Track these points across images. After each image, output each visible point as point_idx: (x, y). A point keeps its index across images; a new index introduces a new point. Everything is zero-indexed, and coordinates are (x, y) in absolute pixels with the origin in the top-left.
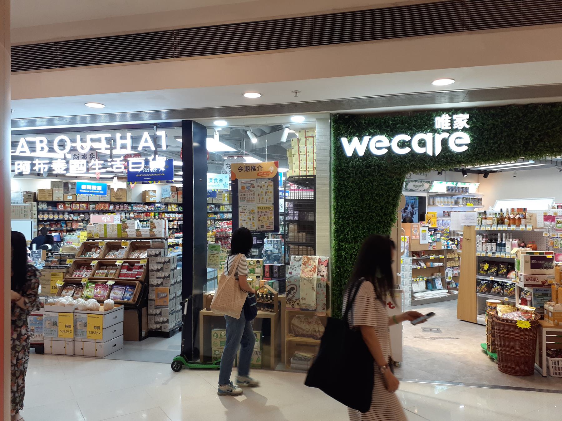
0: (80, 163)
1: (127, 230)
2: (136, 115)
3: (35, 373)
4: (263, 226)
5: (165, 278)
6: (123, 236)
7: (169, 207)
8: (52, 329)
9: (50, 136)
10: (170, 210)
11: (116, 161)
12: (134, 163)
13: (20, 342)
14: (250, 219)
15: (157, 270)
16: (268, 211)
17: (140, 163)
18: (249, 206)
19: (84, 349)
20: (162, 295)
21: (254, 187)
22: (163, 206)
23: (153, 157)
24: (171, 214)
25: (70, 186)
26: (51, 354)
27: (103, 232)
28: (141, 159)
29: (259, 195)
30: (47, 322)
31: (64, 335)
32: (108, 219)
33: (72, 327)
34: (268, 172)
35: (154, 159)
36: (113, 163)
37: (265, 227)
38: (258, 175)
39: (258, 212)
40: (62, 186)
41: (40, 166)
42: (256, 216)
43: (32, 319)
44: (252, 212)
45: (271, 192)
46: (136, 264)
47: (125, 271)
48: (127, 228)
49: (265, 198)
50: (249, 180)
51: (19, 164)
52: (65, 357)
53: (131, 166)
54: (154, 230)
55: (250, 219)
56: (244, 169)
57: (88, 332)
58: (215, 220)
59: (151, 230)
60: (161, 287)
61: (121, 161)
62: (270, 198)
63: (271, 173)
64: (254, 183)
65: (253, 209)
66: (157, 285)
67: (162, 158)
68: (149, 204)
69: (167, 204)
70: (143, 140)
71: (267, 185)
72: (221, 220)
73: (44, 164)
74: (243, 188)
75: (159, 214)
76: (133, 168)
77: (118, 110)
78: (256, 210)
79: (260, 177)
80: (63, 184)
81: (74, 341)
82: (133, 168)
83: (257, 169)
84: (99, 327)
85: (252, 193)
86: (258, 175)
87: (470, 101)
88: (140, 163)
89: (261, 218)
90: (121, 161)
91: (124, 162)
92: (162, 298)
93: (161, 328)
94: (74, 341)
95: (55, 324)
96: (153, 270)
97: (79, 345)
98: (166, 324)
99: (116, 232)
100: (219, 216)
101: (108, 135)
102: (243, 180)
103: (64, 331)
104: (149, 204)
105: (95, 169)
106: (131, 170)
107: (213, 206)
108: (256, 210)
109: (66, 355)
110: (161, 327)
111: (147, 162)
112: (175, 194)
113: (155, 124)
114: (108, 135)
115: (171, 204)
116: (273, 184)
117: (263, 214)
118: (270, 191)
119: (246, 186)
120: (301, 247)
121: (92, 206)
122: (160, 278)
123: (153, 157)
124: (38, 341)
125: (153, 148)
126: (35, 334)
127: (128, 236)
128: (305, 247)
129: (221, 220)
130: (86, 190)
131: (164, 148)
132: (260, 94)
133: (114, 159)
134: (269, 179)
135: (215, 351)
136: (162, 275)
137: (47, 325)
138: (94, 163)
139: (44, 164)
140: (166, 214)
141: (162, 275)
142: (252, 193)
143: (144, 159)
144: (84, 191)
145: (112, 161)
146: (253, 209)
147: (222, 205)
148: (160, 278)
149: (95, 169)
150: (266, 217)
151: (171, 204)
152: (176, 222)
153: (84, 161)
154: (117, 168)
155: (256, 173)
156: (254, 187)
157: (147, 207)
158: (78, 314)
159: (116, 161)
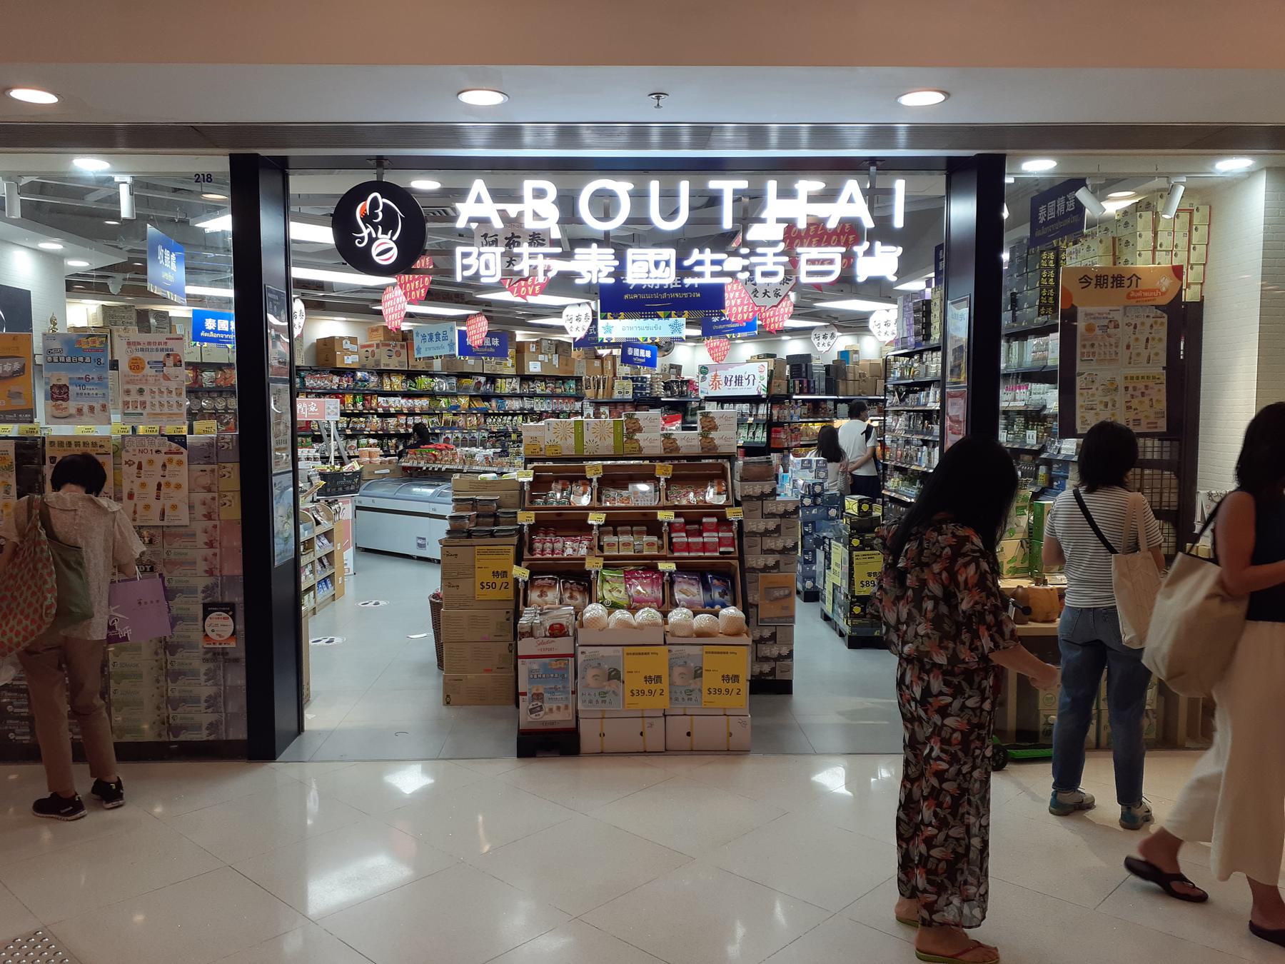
0: (658, 258)
1: (638, 436)
2: (824, 133)
3: (158, 810)
4: (1137, 422)
5: (784, 551)
6: (628, 448)
7: (386, 380)
8: (692, 687)
9: (570, 178)
10: (387, 388)
11: (764, 255)
12: (811, 262)
14: (1106, 406)
15: (767, 533)
16: (1151, 384)
17: (831, 262)
18: (1104, 374)
19: (694, 734)
20: (777, 593)
21: (1117, 326)
22: (374, 379)
23: (866, 245)
24: (391, 400)
25: (152, 321)
26: (602, 753)
27: (571, 441)
28: (835, 253)
29: (1128, 347)
30: (591, 672)
31: (645, 703)
32: (312, 409)
33: (665, 679)
34: (1154, 290)
35: (870, 252)
36: (754, 259)
37: (1144, 422)
38: (1129, 297)
39: (1126, 388)
40: (134, 320)
41: (533, 262)
42: (1121, 398)
43: (535, 667)
44: (1111, 388)
45: (1160, 340)
46: (704, 520)
47: (679, 538)
48: (640, 430)
49: (1145, 353)
50: (1106, 309)
51: (465, 255)
52: (642, 759)
53: (804, 267)
54: (713, 434)
55: (1106, 406)
56: (1094, 282)
57: (705, 692)
58: (487, 414)
59: (704, 435)
60: (773, 575)
61: (775, 255)
62: (1157, 354)
63: (1163, 294)
64: (1118, 316)
65: (1112, 381)
66: (766, 569)
67: (892, 248)
68: (340, 372)
69: (380, 373)
71: (1149, 322)
72: (499, 415)
73: (546, 255)
74: (1090, 329)
75: (364, 399)
76: (810, 274)
77: (774, 116)
78: (1121, 383)
79: (1133, 302)
80: (134, 316)
81: (665, 716)
82: (810, 274)
83: (1127, 283)
84: (659, 677)
85: (1113, 341)
86: (1129, 297)
87: (751, 147)
88: (831, 262)
89: (1135, 403)
90: (775, 255)
91: (786, 259)
92: (777, 599)
93: (773, 671)
94: (665, 716)
95: (614, 675)
96: (754, 534)
97: (678, 726)
98: (787, 662)
99: (610, 441)
100: (494, 403)
101: (743, 184)
102: (1090, 309)
103: (720, 691)
104: (340, 372)
105: (700, 275)
106: (804, 279)
107: (483, 379)
108: (1121, 383)
109: (645, 753)
110: (773, 670)
111: (849, 259)
112: (402, 347)
113: (873, 160)
114: (743, 184)
115: (389, 373)
116: (1165, 320)
117: (1138, 393)
118: (1157, 337)
119: (1097, 323)
120: (1147, 472)
121: (207, 376)
122: (771, 551)
123: (866, 245)
124: (553, 723)
125: (868, 223)
126: (546, 706)
127: (640, 449)
128: (1156, 472)
129: (499, 415)
130: (216, 331)
131: (899, 222)
133: (759, 250)
134: (1157, 307)
135: (1047, 716)
136: (778, 543)
137: (590, 680)
138: (700, 257)
139: (546, 255)
140: (380, 399)
141: (770, 543)
142: (1113, 341)
143: (843, 250)
144: (212, 334)
145: (753, 253)
146: (1112, 381)
147: (501, 376)
148: (771, 551)
149: (700, 275)
150: (1146, 399)
151: (389, 373)
152: (402, 419)
153: (670, 254)
154: (764, 274)
155: (1122, 292)
156: (1117, 326)
157: (336, 379)
158: (674, 648)
159: (764, 255)
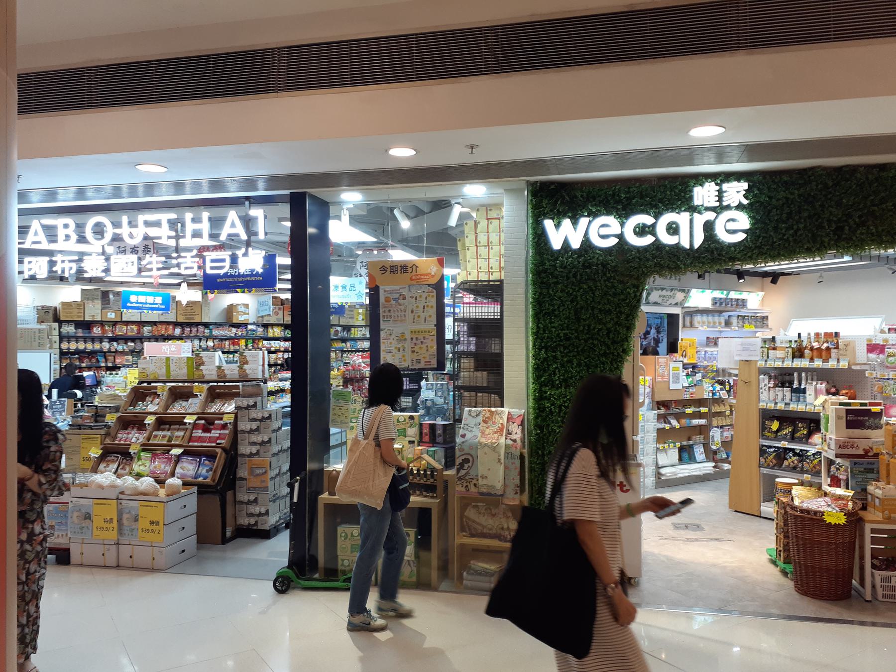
0: (127, 261)
1: (202, 367)
2: (216, 184)
3: (56, 595)
4: (419, 361)
5: (262, 443)
6: (196, 376)
7: (270, 330)
8: (83, 525)
9: (80, 218)
10: (270, 335)
11: (185, 257)
12: (213, 261)
14: (399, 350)
15: (251, 431)
16: (427, 336)
17: (223, 260)
18: (398, 329)
19: (134, 557)
20: (258, 471)
21: (404, 298)
22: (260, 329)
23: (243, 250)
24: (272, 342)
25: (111, 296)
26: (81, 565)
27: (164, 370)
28: (226, 255)
29: (412, 312)
30: (76, 514)
31: (103, 535)
32: (173, 349)
33: (115, 521)
34: (427, 275)
35: (245, 254)
36: (180, 260)
37: (422, 362)
38: (412, 279)
39: (412, 339)
40: (99, 297)
41: (63, 265)
42: (408, 345)
43: (51, 509)
44: (402, 338)
45: (432, 307)
46: (216, 422)
47: (199, 433)
48: (203, 364)
49: (423, 316)
50: (397, 287)
51: (30, 262)
52: (104, 570)
53: (209, 265)
54: (246, 367)
55: (399, 350)
56: (389, 270)
57: (140, 531)
58: (343, 352)
59: (241, 368)
60: (256, 458)
61: (192, 257)
62: (430, 316)
63: (433, 276)
64: (405, 292)
65: (403, 334)
66: (251, 455)
67: (258, 251)
68: (238, 326)
69: (266, 326)
71: (425, 295)
72: (352, 351)
73: (70, 261)
74: (387, 300)
75: (254, 342)
76: (212, 268)
77: (188, 176)
78: (408, 336)
79: (414, 282)
80: (100, 294)
81: (118, 544)
82: (212, 268)
83: (410, 270)
84: (158, 522)
85: (402, 308)
86: (412, 279)
87: (750, 160)
88: (223, 260)
89: (416, 349)
90: (192, 257)
91: (198, 259)
92: (258, 475)
93: (256, 523)
94: (118, 544)
95: (88, 517)
96: (244, 432)
97: (125, 551)
98: (265, 518)
99: (185, 371)
100: (348, 344)
101: (173, 216)
102: (388, 288)
103: (103, 528)
104: (238, 326)
105: (151, 270)
106: (209, 271)
107: (339, 329)
108: (408, 336)
109: (105, 567)
110: (256, 522)
111: (234, 259)
112: (280, 309)
113: (247, 198)
114: (173, 216)
115: (272, 325)
116: (434, 294)
117: (419, 342)
118: (430, 305)
119: (392, 296)
120: (480, 395)
121: (146, 330)
122: (254, 444)
123: (243, 250)
124: (60, 544)
125: (244, 237)
126: (56, 533)
127: (203, 376)
128: (486, 395)
129: (352, 351)
130: (137, 303)
131: (261, 236)
133: (182, 254)
134: (429, 285)
135: (343, 560)
136: (258, 438)
137: (75, 519)
138: (150, 259)
139: (70, 261)
140: (265, 342)
141: (258, 438)
142: (402, 308)
143: (230, 253)
144: (135, 305)
145: (179, 257)
146: (403, 334)
147: (355, 327)
148: (254, 444)
149: (151, 270)
150: (424, 346)
151: (272, 325)
152: (280, 355)
153: (134, 257)
154: (186, 268)
155: (408, 276)
156: (404, 298)
157: (234, 330)
158: (124, 502)
159: (185, 257)
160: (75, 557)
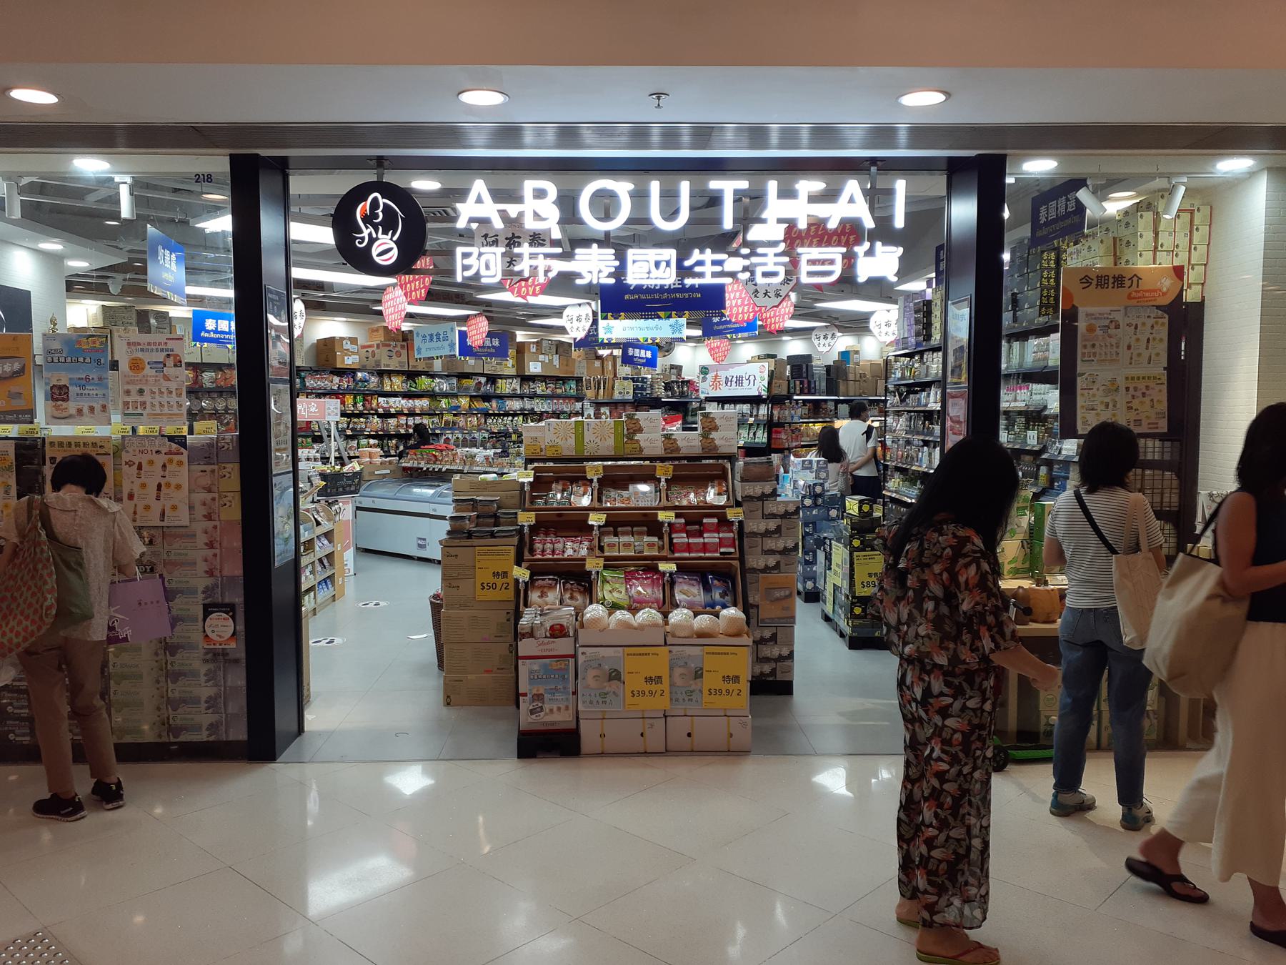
0: (659, 258)
1: (638, 436)
2: (824, 134)
3: (158, 810)
4: (1138, 422)
5: (785, 551)
6: (629, 448)
7: (386, 381)
8: (693, 687)
9: (570, 179)
10: (387, 388)
11: (764, 255)
12: (812, 262)
13: (926, 712)
14: (1107, 406)
15: (767, 533)
16: (1152, 384)
17: (832, 262)
18: (1105, 374)
19: (694, 735)
20: (778, 594)
21: (1117, 327)
22: (374, 379)
23: (867, 245)
24: (392, 400)
25: (153, 321)
26: (602, 754)
27: (572, 442)
28: (836, 253)
29: (1129, 347)
30: (591, 673)
31: (645, 703)
32: (313, 410)
33: (666, 680)
34: (1155, 291)
35: (870, 253)
36: (754, 260)
37: (1145, 423)
38: (1129, 297)
39: (1127, 389)
40: (134, 321)
41: (534, 262)
42: (1122, 398)
43: (536, 667)
44: (1112, 388)
45: (1161, 340)
46: (705, 520)
47: (680, 538)
48: (640, 430)
49: (1146, 354)
50: (1107, 309)
51: (466, 255)
52: (642, 759)
53: (804, 268)
54: (714, 435)
55: (1107, 406)
56: (1094, 282)
57: (706, 692)
58: (487, 415)
59: (705, 436)
60: (774, 576)
61: (776, 255)
62: (1158, 355)
63: (1164, 294)
64: (1119, 317)
65: (1113, 382)
66: (767, 569)
67: (893, 248)
68: (341, 372)
69: (381, 374)
70: (472, 196)
71: (1150, 322)
72: (499, 415)
73: (546, 256)
74: (1091, 329)
75: (365, 400)
76: (810, 274)
77: (774, 116)
78: (1122, 383)
79: (1134, 302)
80: (134, 316)
81: (666, 717)
82: (810, 274)
83: (1128, 283)
84: (660, 678)
85: (1114, 341)
86: (1129, 297)
87: (751, 148)
88: (832, 262)
89: (1135, 404)
90: (776, 255)
91: (786, 259)
92: (778, 599)
93: (774, 672)
94: (666, 717)
95: (615, 676)
96: (754, 534)
97: (679, 727)
98: (787, 663)
99: (611, 441)
100: (494, 404)
101: (743, 184)
102: (1091, 310)
103: (721, 691)
104: (341, 372)
105: (701, 275)
106: (805, 279)
107: (483, 380)
108: (1122, 383)
109: (646, 753)
110: (774, 671)
111: (850, 259)
112: (402, 347)
113: (873, 161)
114: (743, 184)
115: (390, 373)
116: (1166, 320)
117: (1139, 394)
118: (1158, 337)
119: (1098, 323)
120: (1148, 472)
121: (207, 376)
122: (772, 552)
123: (867, 245)
124: (553, 723)
125: (869, 223)
126: (547, 707)
127: (641, 450)
128: (1157, 472)
129: (499, 415)
130: (216, 331)
131: (899, 223)
132: (57, 95)
133: (760, 250)
134: (1158, 307)
135: (1048, 717)
136: (779, 544)
137: (590, 681)
138: (701, 257)
139: (546, 256)
140: (381, 400)
141: (771, 544)
142: (1114, 341)
143: (844, 250)
144: (212, 335)
145: (753, 254)
146: (1113, 382)
147: (501, 377)
148: (772, 552)
149: (701, 275)
150: (1147, 400)
151: (390, 373)
152: (403, 420)
153: (671, 254)
154: (765, 274)
155: (1123, 292)
156: (1117, 327)
157: (336, 379)
158: (674, 649)
159: (764, 255)
160: (589, 734)
